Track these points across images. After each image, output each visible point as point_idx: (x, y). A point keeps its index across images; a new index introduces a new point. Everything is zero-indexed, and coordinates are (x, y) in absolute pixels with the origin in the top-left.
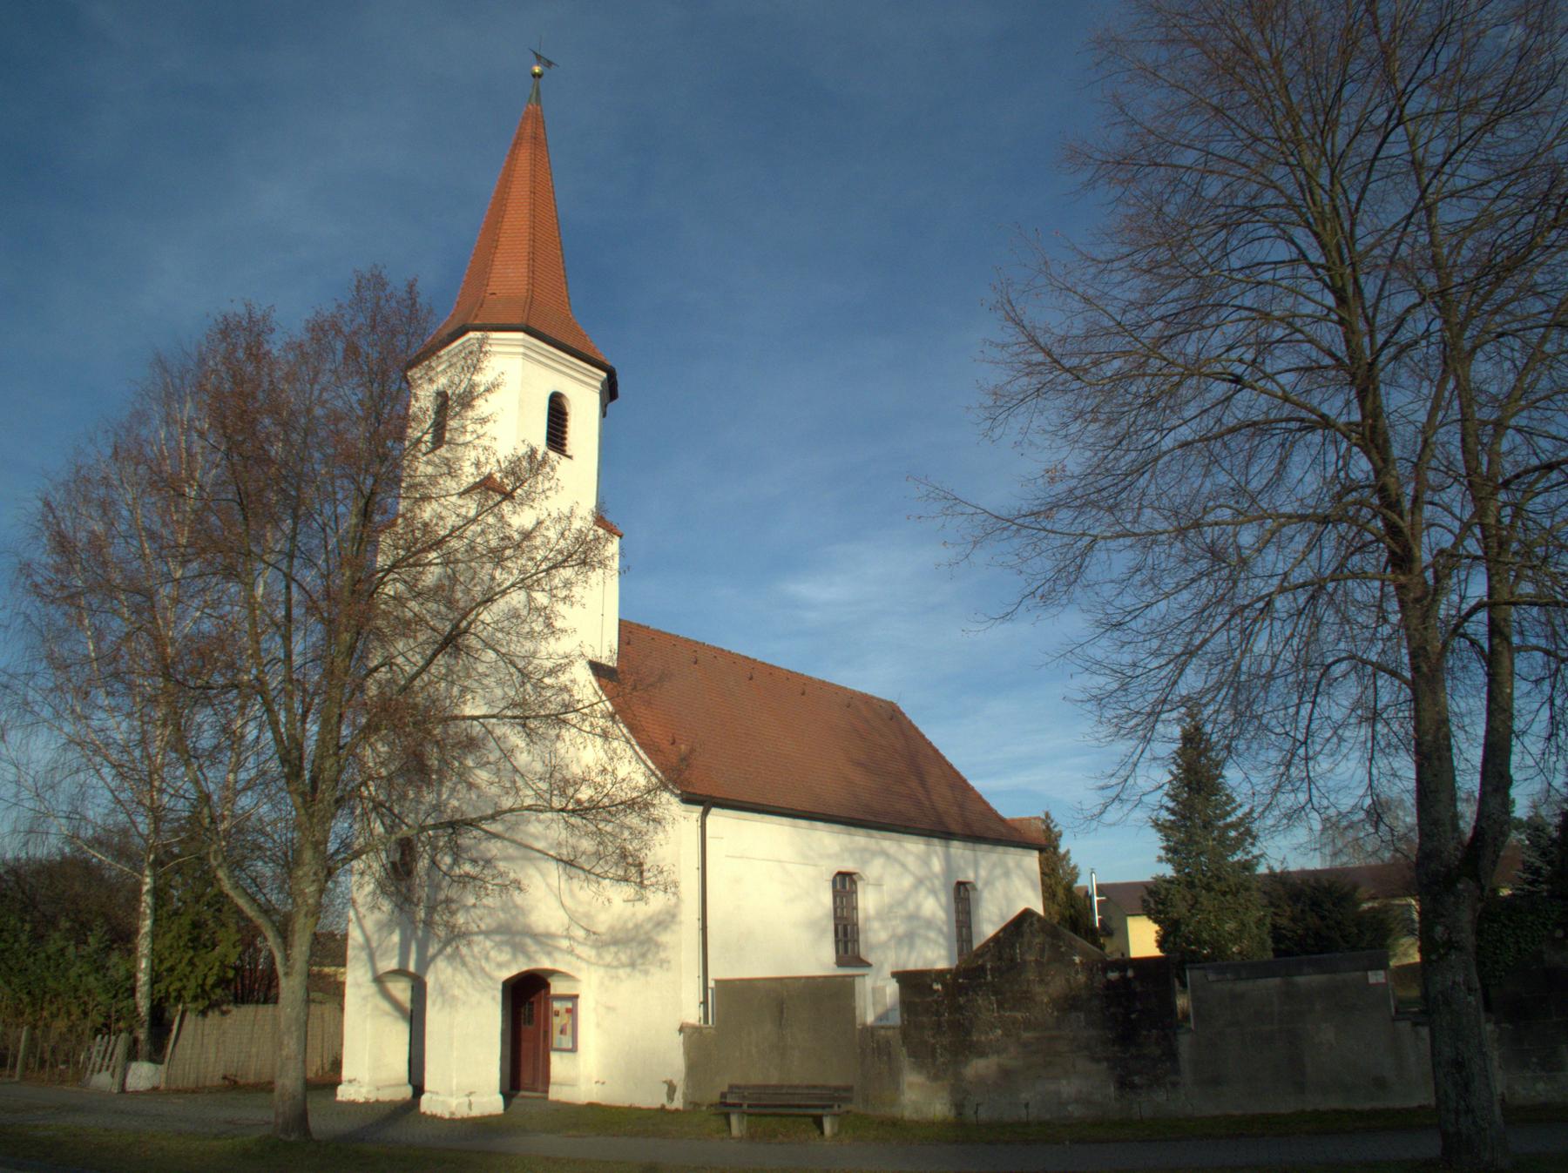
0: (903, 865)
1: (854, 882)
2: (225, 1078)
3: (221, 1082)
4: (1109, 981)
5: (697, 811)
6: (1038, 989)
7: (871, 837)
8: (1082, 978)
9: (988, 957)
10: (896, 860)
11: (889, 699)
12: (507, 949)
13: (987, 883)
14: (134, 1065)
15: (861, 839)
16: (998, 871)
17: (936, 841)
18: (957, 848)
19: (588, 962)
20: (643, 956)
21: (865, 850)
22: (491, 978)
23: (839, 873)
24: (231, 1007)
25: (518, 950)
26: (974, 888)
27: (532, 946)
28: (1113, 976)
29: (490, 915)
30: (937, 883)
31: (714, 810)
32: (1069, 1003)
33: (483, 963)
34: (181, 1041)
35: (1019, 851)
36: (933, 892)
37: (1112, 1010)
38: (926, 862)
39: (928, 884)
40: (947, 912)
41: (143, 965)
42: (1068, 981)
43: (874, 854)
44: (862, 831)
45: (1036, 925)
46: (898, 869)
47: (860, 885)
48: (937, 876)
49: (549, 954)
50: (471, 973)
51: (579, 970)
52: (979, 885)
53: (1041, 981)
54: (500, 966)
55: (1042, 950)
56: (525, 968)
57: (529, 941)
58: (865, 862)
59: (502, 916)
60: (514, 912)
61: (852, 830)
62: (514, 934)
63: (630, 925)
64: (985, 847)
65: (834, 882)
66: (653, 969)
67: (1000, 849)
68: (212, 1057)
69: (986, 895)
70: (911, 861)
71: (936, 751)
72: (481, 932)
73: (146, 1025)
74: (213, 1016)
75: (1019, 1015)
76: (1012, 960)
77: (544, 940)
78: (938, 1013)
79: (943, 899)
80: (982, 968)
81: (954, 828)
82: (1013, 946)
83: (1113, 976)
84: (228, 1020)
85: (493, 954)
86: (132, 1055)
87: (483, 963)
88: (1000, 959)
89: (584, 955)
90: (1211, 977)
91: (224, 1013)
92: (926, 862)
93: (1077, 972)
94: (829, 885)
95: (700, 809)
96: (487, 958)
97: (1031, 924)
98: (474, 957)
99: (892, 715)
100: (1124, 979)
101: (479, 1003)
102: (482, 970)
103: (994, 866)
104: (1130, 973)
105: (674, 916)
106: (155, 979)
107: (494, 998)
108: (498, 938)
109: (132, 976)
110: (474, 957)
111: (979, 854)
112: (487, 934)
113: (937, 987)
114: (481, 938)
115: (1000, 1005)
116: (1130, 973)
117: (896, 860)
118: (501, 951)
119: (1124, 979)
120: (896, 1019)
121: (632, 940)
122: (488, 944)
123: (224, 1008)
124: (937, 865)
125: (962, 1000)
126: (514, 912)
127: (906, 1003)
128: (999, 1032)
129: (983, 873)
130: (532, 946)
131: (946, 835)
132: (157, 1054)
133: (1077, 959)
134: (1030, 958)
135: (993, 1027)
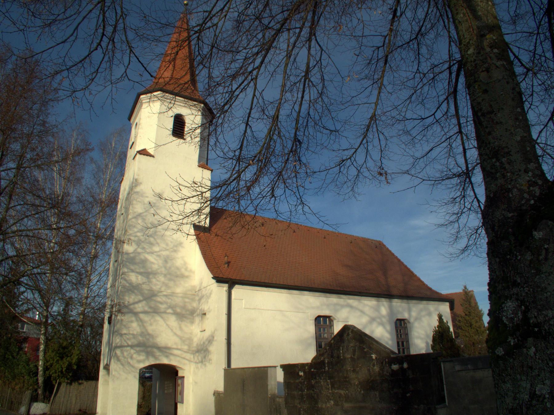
0: (363, 312)
1: (405, 323)
2: (80, 410)
3: (78, 412)
4: (393, 370)
5: (225, 287)
6: (352, 375)
7: (341, 298)
8: (377, 369)
9: (326, 356)
10: (356, 309)
11: (378, 239)
12: (144, 354)
13: (416, 319)
14: (35, 404)
15: (334, 299)
16: (424, 313)
17: (383, 299)
18: (397, 303)
19: (190, 361)
20: (205, 357)
21: (336, 305)
22: (133, 367)
23: (319, 317)
24: (83, 381)
25: (149, 354)
26: (409, 322)
27: (158, 353)
28: (395, 367)
29: (134, 338)
30: (384, 320)
31: (237, 286)
32: (370, 385)
33: (129, 360)
34: (58, 395)
35: (437, 303)
36: (382, 324)
37: (395, 390)
38: (377, 309)
39: (378, 320)
40: (391, 333)
41: (40, 363)
42: (369, 370)
43: (343, 306)
44: (311, 293)
45: (351, 335)
46: (358, 313)
47: (335, 322)
48: (384, 316)
49: (167, 357)
50: (122, 365)
51: (184, 364)
52: (412, 320)
53: (354, 371)
54: (139, 362)
55: (354, 351)
56: (153, 363)
57: (155, 350)
58: (336, 311)
59: (141, 338)
60: (148, 337)
61: (328, 295)
62: (146, 345)
63: (202, 343)
64: (414, 301)
65: (396, 323)
66: (207, 364)
67: (425, 302)
68: (74, 402)
69: (416, 324)
70: (367, 309)
71: (399, 260)
72: (128, 346)
73: (42, 387)
74: (75, 385)
75: (342, 392)
76: (338, 357)
77: (165, 350)
78: (302, 390)
79: (388, 327)
80: (323, 363)
81: (395, 292)
82: (338, 349)
83: (395, 367)
84: (82, 387)
85: (135, 356)
86: (34, 399)
87: (129, 360)
88: (332, 356)
89: (188, 358)
90: (458, 368)
91: (80, 384)
92: (377, 309)
93: (374, 365)
94: (313, 322)
95: (227, 285)
96: (132, 358)
97: (348, 335)
98: (124, 357)
99: (379, 247)
100: (402, 368)
101: (126, 378)
102: (129, 363)
103: (421, 310)
104: (405, 365)
105: (213, 337)
106: (46, 369)
107: (135, 377)
108: (138, 349)
109: (37, 367)
110: (124, 357)
111: (411, 305)
112: (132, 347)
113: (301, 374)
114: (129, 348)
115: (333, 386)
116: (405, 365)
117: (356, 309)
118: (139, 355)
119: (402, 368)
120: (283, 393)
121: (202, 350)
122: (132, 351)
123: (80, 381)
124: (384, 311)
125: (313, 382)
126: (148, 337)
127: (287, 383)
128: (332, 402)
129: (414, 314)
130: (158, 353)
131: (389, 296)
132: (46, 399)
133: (374, 356)
134: (348, 356)
135: (329, 399)
